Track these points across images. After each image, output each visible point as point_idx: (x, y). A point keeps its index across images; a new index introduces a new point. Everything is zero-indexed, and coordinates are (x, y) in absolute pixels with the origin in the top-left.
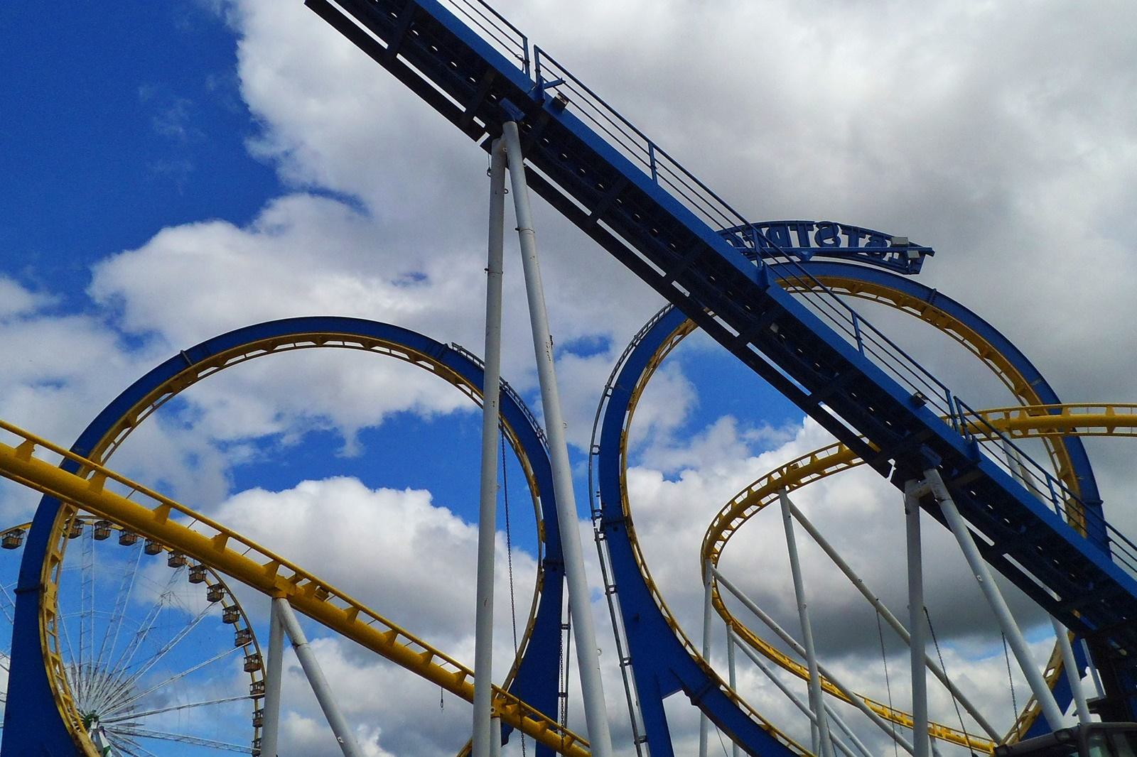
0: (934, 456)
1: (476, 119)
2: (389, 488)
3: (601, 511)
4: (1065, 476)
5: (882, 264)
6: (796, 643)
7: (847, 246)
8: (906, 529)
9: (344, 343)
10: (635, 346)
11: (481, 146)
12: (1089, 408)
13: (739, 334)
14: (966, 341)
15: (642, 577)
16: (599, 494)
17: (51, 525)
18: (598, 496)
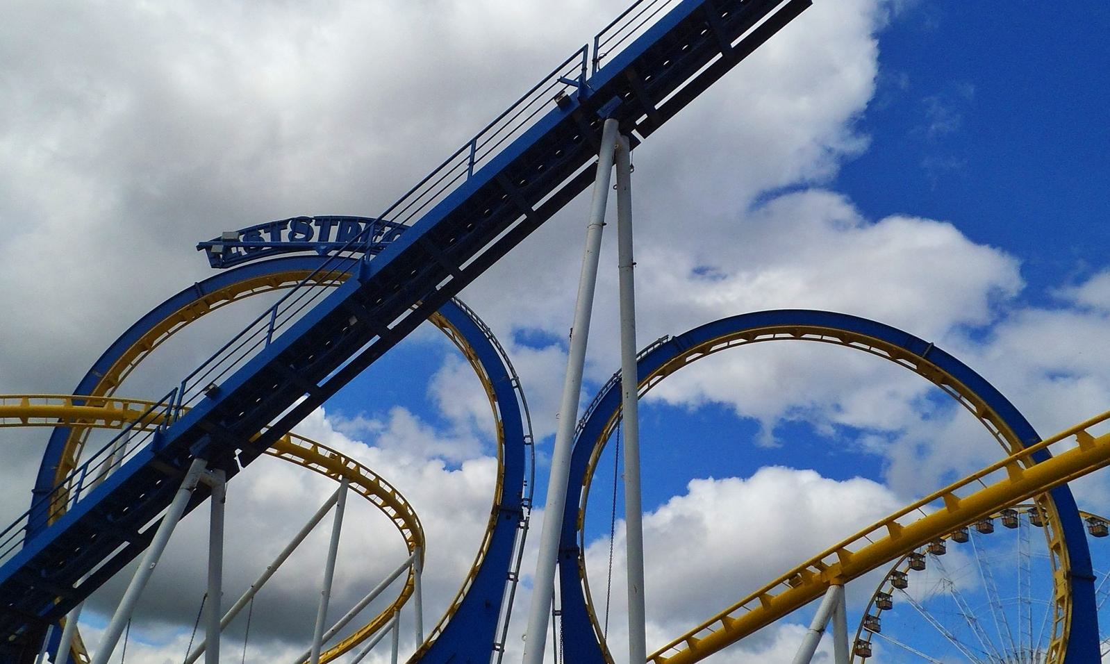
0: (197, 446)
1: (645, 116)
2: (730, 478)
3: (523, 505)
4: (68, 465)
5: (264, 253)
6: (331, 630)
7: (317, 241)
8: (225, 517)
9: (998, 433)
10: (489, 338)
11: (645, 138)
12: (49, 399)
13: (534, 210)
14: (170, 331)
15: (484, 561)
16: (524, 483)
17: (1060, 514)
18: (526, 482)
